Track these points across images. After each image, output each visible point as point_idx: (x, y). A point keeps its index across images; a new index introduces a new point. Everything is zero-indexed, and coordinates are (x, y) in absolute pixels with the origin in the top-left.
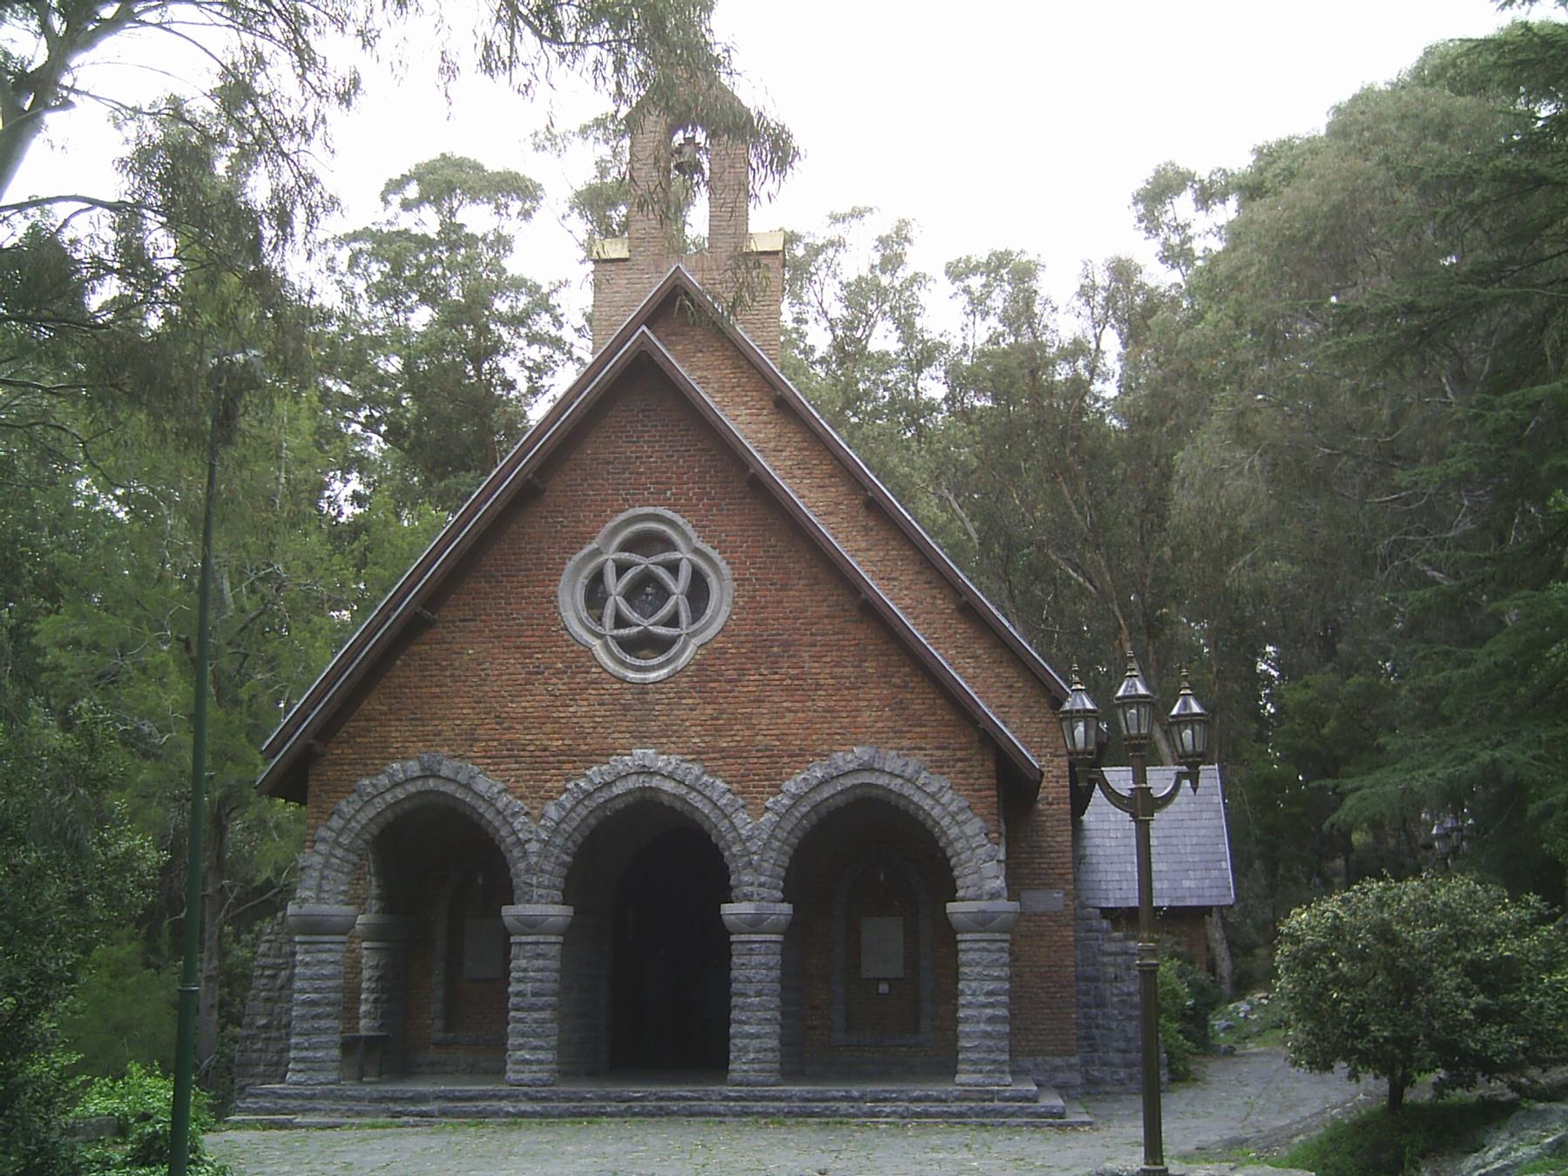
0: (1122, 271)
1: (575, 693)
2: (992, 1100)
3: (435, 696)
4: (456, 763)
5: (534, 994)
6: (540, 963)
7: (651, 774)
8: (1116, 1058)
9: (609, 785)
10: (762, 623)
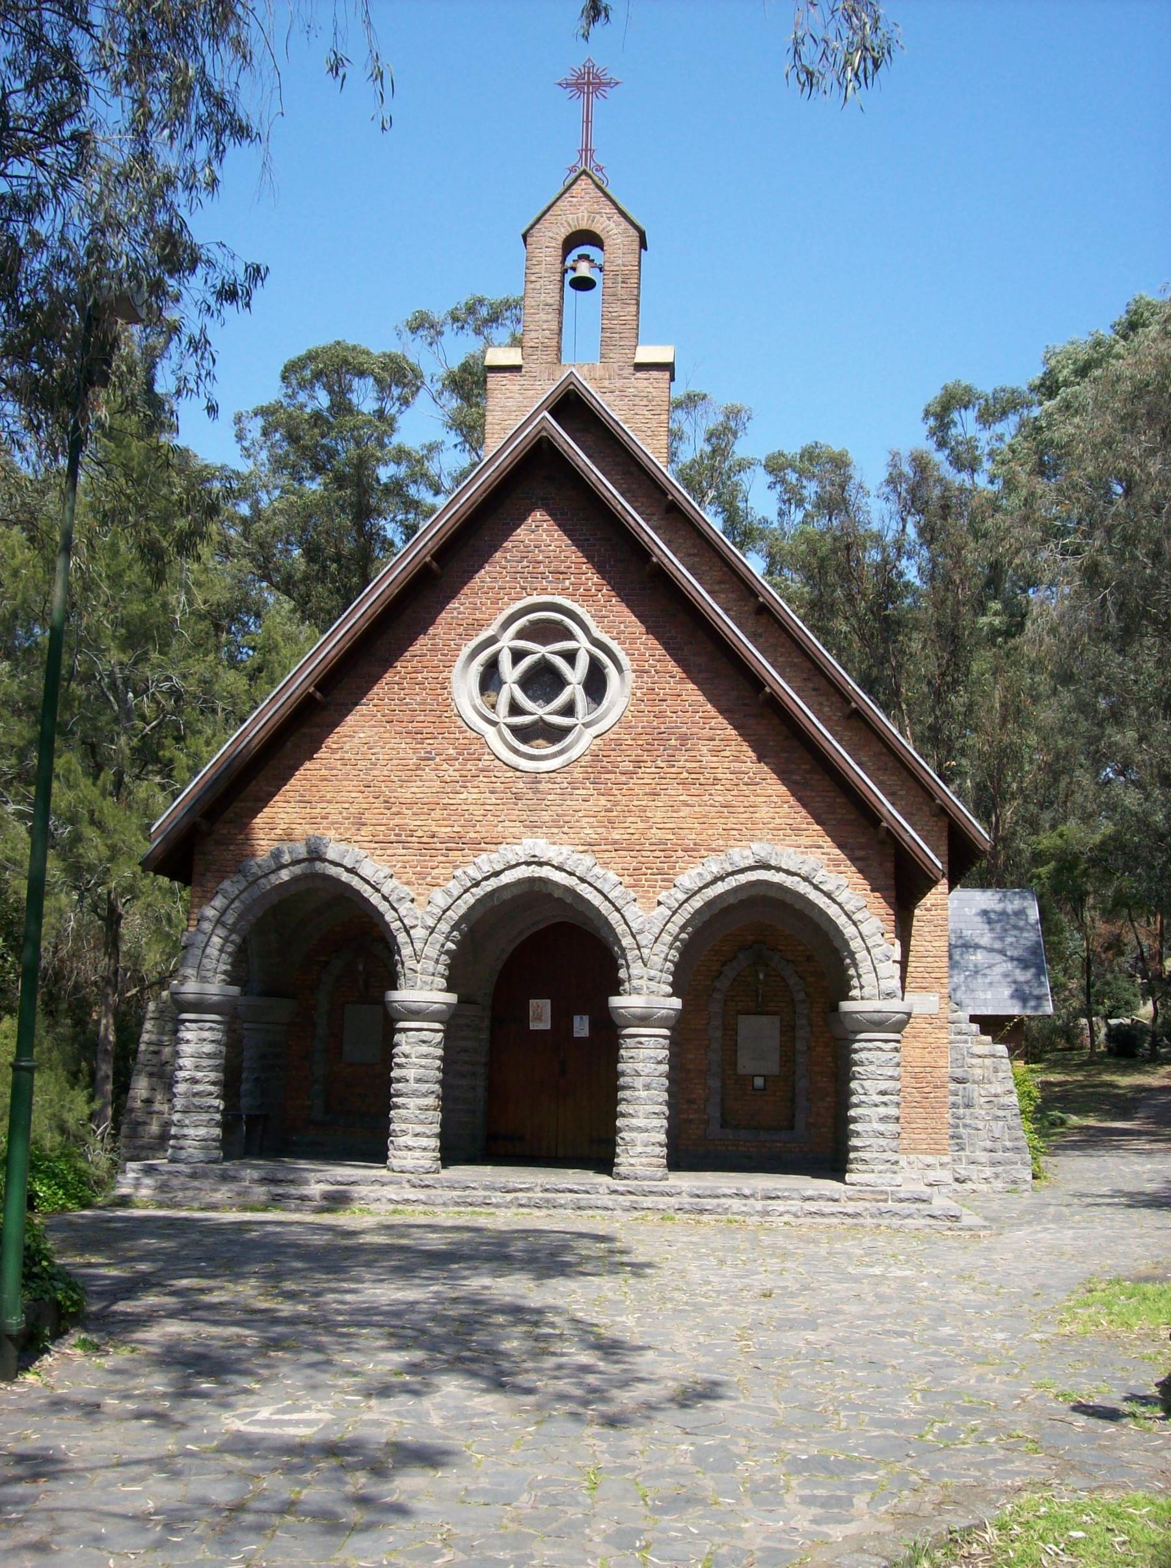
0: (921, 464)
1: (465, 781)
2: (886, 1201)
3: (324, 779)
4: (343, 846)
5: (418, 1081)
6: (424, 1049)
7: (541, 864)
8: (983, 1157)
9: (497, 874)
10: (660, 715)
